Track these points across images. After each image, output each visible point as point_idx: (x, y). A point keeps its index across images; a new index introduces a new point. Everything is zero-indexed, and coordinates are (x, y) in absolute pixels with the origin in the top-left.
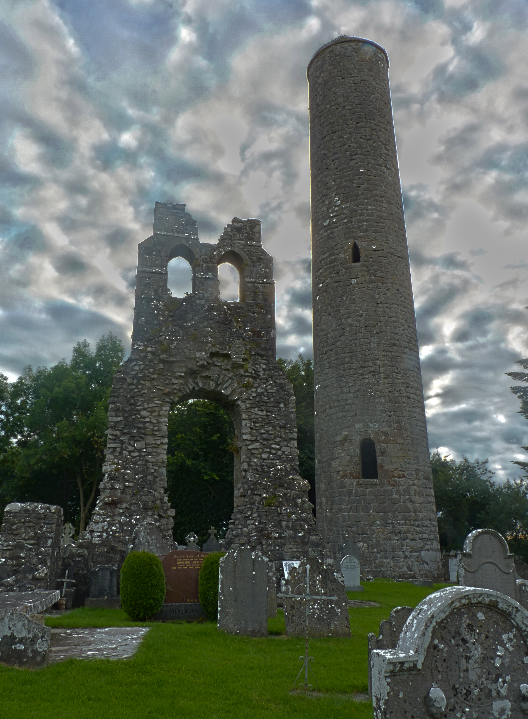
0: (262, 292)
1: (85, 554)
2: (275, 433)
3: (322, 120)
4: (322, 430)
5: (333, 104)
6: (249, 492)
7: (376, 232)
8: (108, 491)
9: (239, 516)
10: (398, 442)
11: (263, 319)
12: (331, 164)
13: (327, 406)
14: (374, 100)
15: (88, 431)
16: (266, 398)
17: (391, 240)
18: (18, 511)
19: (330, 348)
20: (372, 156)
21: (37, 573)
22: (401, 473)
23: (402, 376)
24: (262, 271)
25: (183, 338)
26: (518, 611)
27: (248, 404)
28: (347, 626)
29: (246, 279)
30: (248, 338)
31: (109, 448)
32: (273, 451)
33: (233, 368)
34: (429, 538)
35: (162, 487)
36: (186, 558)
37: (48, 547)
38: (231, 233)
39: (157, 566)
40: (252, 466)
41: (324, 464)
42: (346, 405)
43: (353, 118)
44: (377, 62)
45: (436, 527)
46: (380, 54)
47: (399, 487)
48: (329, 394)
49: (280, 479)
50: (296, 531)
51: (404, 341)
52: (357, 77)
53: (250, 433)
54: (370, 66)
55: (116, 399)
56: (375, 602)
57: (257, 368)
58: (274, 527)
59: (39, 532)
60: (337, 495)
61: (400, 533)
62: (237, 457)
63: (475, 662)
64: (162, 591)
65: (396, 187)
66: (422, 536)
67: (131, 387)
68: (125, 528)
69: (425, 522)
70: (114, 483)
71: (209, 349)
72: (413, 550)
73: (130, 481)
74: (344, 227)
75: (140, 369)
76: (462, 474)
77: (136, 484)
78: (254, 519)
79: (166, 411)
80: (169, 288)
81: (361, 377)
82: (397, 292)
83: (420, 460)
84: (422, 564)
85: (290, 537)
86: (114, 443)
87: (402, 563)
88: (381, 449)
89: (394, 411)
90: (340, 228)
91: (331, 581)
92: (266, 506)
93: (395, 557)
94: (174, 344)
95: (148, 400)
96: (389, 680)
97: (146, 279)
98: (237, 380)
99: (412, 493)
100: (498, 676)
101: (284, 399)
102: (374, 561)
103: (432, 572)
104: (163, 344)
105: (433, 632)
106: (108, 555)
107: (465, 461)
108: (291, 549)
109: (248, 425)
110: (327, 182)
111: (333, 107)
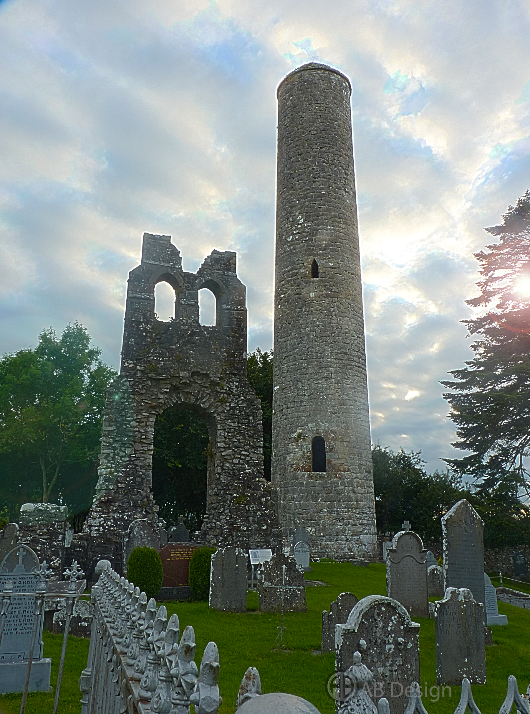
0: (236, 318)
1: (85, 545)
2: (245, 442)
3: (289, 141)
4: (280, 427)
5: (300, 127)
6: (222, 492)
7: (333, 250)
8: (104, 491)
9: (213, 512)
10: (345, 440)
11: (236, 342)
12: (296, 184)
13: (285, 406)
14: (337, 127)
15: (54, 417)
16: (238, 412)
17: (346, 258)
18: (32, 511)
19: (289, 354)
20: (333, 180)
21: (52, 563)
22: (346, 467)
23: (351, 382)
24: (237, 298)
25: (169, 359)
26: (399, 606)
27: (223, 416)
28: (304, 604)
29: (223, 306)
30: (224, 359)
31: (103, 453)
32: (243, 457)
33: (211, 385)
34: (368, 523)
35: (148, 487)
36: (178, 551)
37: (59, 541)
38: (210, 264)
39: (157, 558)
40: (225, 470)
41: (279, 458)
42: (301, 406)
43: (318, 142)
44: (341, 90)
45: (374, 514)
46: (345, 83)
47: (344, 479)
48: (286, 396)
49: (248, 481)
50: (261, 525)
51: (353, 350)
52: (323, 104)
53: (224, 441)
54: (335, 94)
55: (109, 411)
56: (322, 581)
57: (231, 385)
58: (243, 521)
59: (51, 528)
60: (290, 485)
61: (343, 519)
62: (211, 460)
63: (380, 629)
64: (161, 578)
65: (353, 209)
66: (362, 522)
67: (122, 400)
68: (119, 523)
69: (364, 510)
70: (108, 484)
71: (191, 369)
72: (353, 534)
73: (122, 482)
74: (305, 244)
75: (130, 385)
76: (399, 463)
77: (127, 485)
78: (226, 515)
79: (152, 422)
80: (155, 312)
81: (315, 382)
82: (349, 306)
83: (363, 456)
84: (361, 546)
85: (256, 530)
86: (108, 449)
87: (344, 545)
88: (329, 445)
89: (343, 413)
90: (301, 244)
91: (294, 571)
92: (236, 504)
93: (338, 540)
94: (161, 364)
95: (136, 412)
96: (343, 637)
97: (136, 304)
98: (214, 395)
99: (355, 485)
100: (389, 634)
101: (252, 413)
102: (321, 544)
103: (369, 552)
104: (151, 364)
105: (362, 616)
106: (104, 546)
107: (402, 452)
108: (256, 539)
109: (223, 434)
110: (292, 200)
111: (299, 131)
